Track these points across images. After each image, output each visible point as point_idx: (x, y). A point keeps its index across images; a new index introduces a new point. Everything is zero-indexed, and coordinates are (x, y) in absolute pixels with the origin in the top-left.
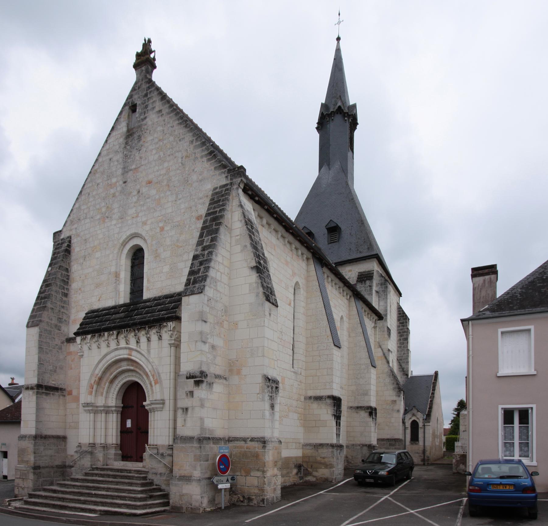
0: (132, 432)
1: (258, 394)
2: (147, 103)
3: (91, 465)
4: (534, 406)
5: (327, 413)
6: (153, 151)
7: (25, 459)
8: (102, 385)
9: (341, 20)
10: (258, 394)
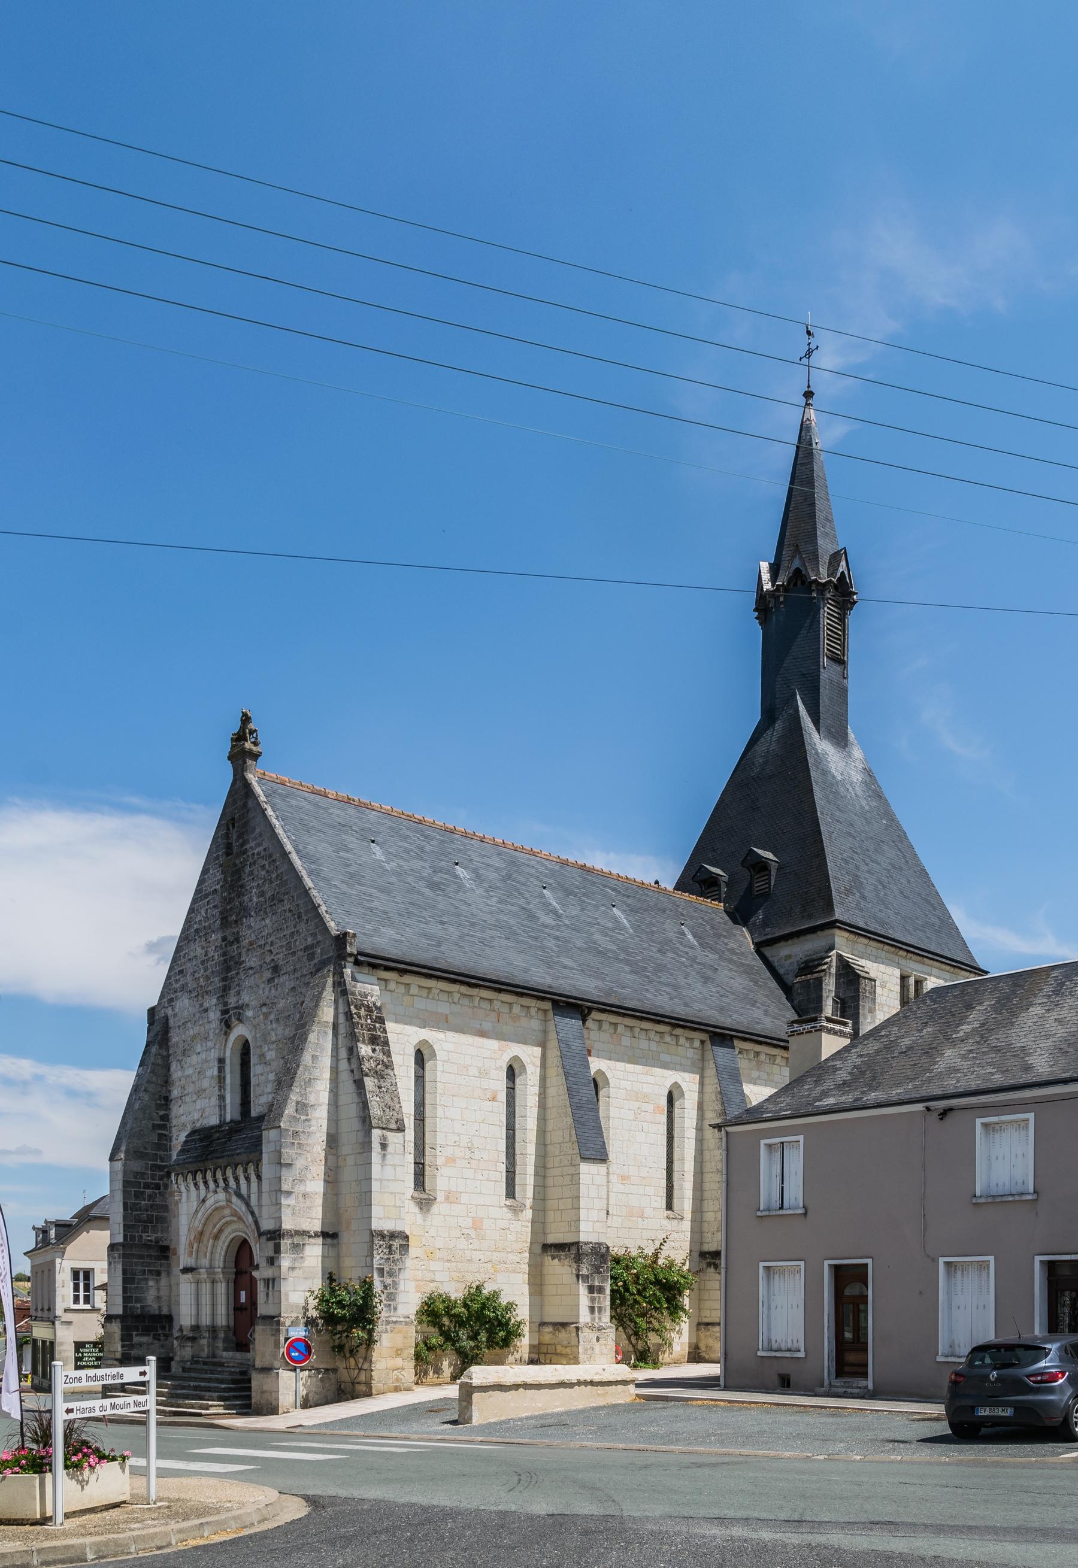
0: (246, 1309)
1: (367, 1256)
2: (223, 943)
3: (193, 1357)
4: (869, 1261)
5: (572, 1273)
6: (190, 1069)
7: (112, 1349)
8: (205, 1242)
9: (813, 346)
10: (367, 1256)
